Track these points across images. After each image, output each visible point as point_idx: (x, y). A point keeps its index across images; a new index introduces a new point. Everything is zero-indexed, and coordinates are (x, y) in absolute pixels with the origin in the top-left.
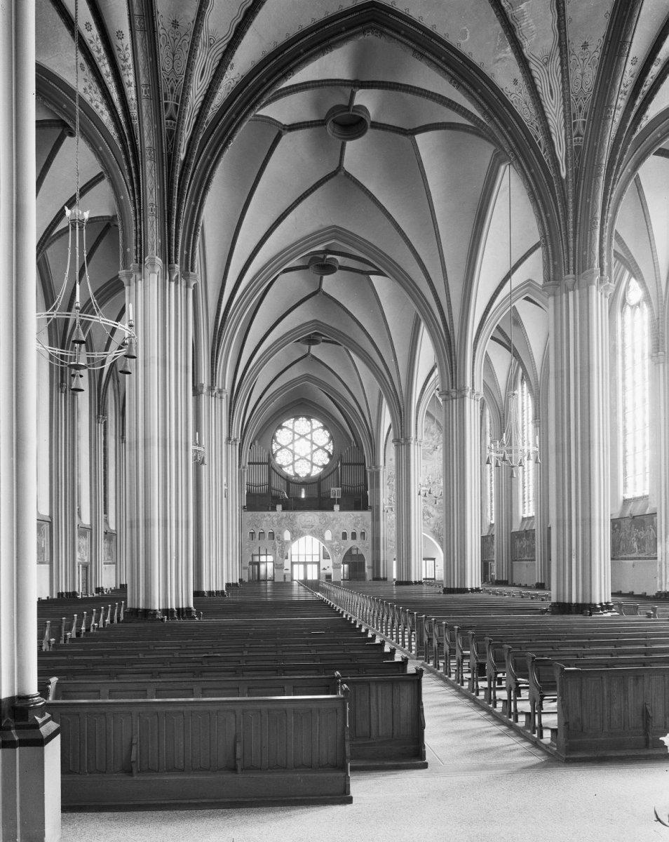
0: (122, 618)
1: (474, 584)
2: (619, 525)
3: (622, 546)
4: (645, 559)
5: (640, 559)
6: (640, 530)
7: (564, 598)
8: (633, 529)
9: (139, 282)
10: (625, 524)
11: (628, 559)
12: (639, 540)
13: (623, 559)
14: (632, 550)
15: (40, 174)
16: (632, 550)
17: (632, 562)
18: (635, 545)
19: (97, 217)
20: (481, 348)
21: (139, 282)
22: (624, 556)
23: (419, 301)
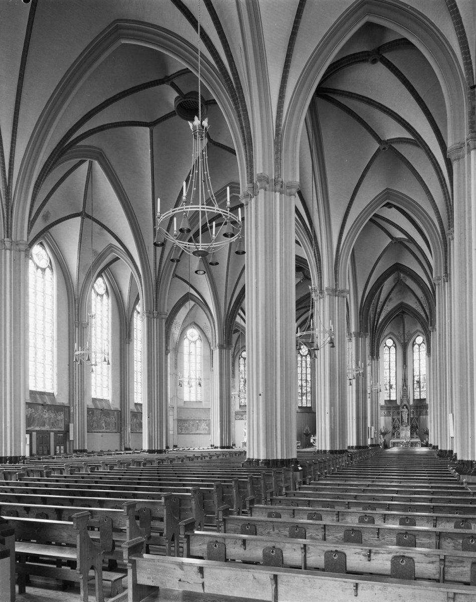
0: (34, 452)
1: (251, 454)
2: (93, 413)
3: (95, 425)
4: (110, 432)
5: (106, 432)
6: (107, 417)
7: (76, 448)
8: (102, 416)
9: (446, 283)
10: (97, 413)
11: (100, 432)
12: (106, 423)
13: (95, 432)
14: (102, 428)
15: (322, 81)
16: (102, 428)
17: (101, 434)
18: (104, 425)
19: (107, 124)
20: (343, 278)
21: (446, 283)
22: (96, 431)
23: (423, 218)
